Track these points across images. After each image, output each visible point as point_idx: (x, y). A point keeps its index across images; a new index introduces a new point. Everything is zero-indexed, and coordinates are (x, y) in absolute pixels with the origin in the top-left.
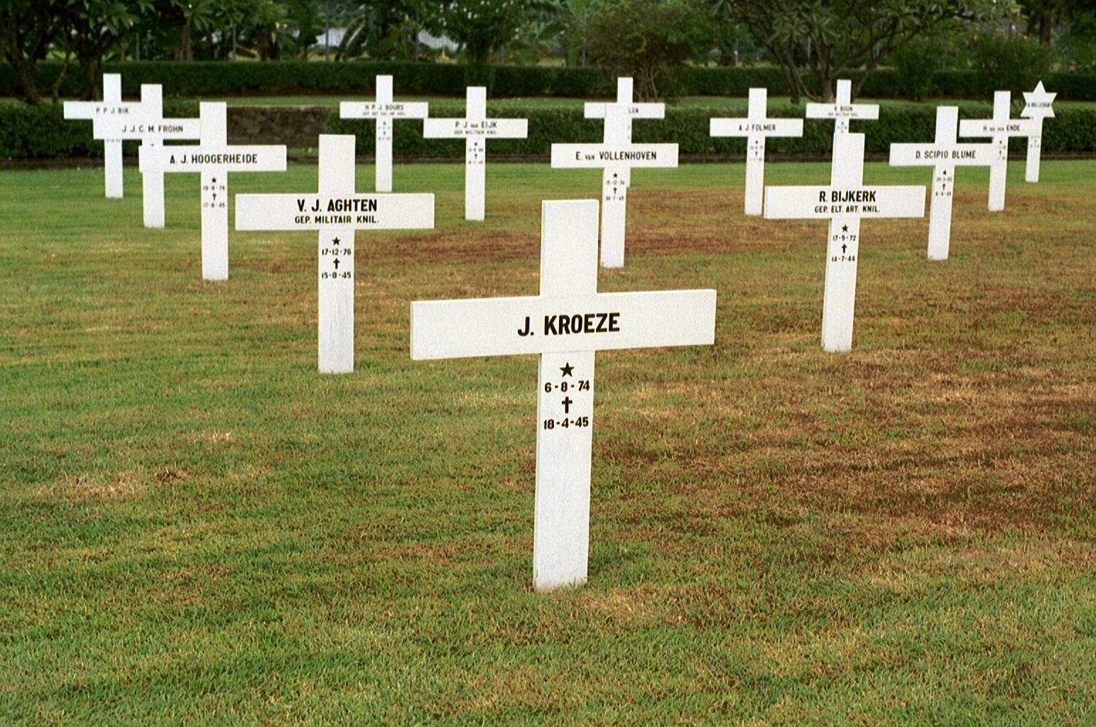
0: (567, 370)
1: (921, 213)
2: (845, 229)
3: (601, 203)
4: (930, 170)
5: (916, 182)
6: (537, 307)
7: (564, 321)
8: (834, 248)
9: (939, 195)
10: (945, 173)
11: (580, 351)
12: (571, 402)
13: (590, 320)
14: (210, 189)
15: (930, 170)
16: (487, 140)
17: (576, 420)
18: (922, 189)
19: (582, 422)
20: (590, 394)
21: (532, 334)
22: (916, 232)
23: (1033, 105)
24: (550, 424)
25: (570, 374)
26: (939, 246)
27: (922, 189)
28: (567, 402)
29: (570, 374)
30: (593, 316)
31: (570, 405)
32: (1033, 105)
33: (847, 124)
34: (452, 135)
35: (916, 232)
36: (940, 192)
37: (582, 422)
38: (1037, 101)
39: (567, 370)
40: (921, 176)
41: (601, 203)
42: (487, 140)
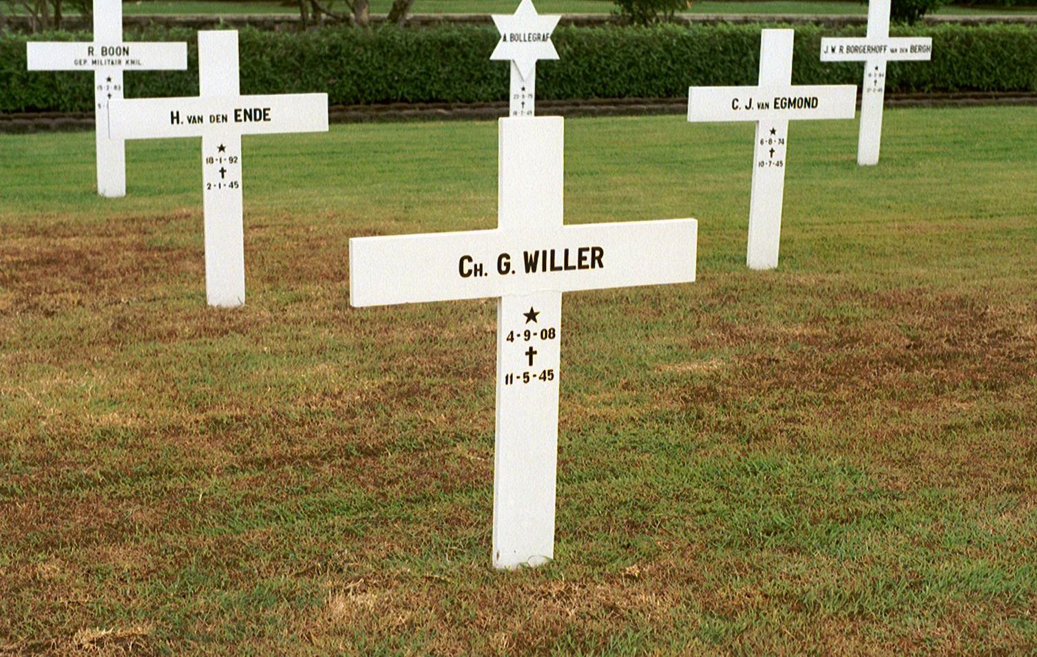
0: (532, 316)
1: (851, 114)
2: (773, 132)
3: (860, 91)
4: (861, 65)
5: (849, 80)
6: (482, 245)
7: (597, 254)
8: (761, 153)
9: (519, 114)
10: (877, 68)
11: (546, 293)
12: (536, 353)
13: (584, 254)
14: (104, 90)
15: (861, 65)
16: (125, 73)
17: (539, 374)
18: (855, 87)
19: (547, 375)
20: (555, 345)
21: (513, 272)
22: (847, 132)
23: (513, 37)
24: (509, 379)
25: (535, 320)
26: (869, 150)
27: (855, 87)
28: (531, 353)
29: (535, 320)
30: (587, 249)
31: (534, 356)
32: (513, 37)
33: (119, 80)
34: (70, 66)
35: (847, 132)
36: (519, 111)
37: (547, 375)
38: (522, 30)
39: (532, 316)
40: (851, 74)
41: (860, 91)
42: (125, 73)
